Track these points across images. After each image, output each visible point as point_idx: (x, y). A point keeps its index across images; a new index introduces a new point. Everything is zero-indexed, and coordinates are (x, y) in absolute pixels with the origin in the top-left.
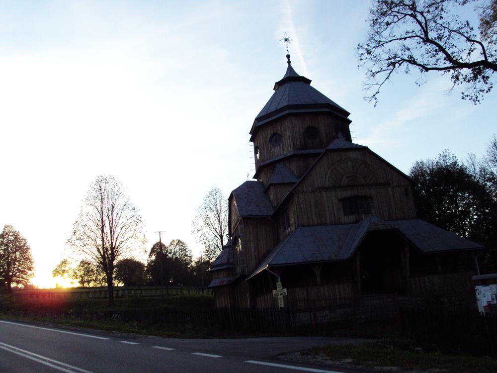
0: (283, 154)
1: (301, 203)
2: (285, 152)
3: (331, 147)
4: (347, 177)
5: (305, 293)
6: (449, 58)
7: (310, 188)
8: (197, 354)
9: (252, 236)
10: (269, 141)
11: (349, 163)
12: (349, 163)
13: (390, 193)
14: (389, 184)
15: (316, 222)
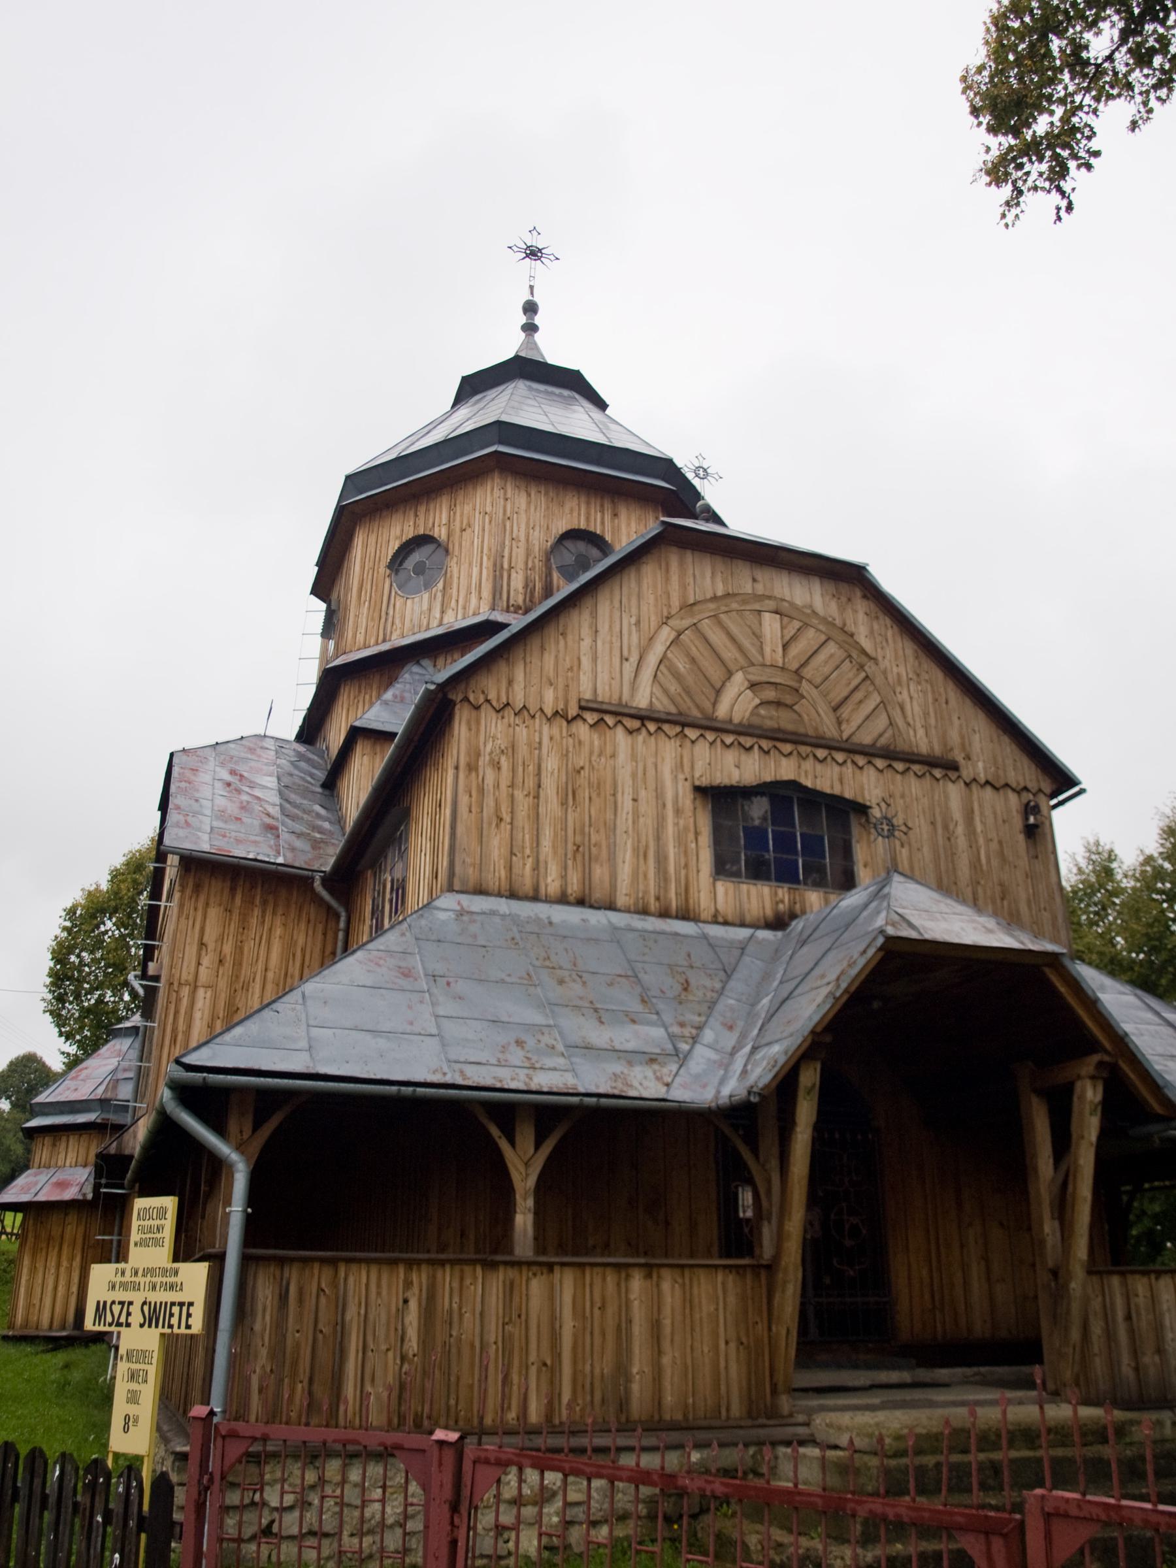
0: (440, 624)
1: (484, 760)
5: (413, 1305)
6: (716, 953)
7: (549, 696)
10: (390, 566)
11: (767, 616)
13: (957, 813)
14: (951, 766)
15: (552, 883)
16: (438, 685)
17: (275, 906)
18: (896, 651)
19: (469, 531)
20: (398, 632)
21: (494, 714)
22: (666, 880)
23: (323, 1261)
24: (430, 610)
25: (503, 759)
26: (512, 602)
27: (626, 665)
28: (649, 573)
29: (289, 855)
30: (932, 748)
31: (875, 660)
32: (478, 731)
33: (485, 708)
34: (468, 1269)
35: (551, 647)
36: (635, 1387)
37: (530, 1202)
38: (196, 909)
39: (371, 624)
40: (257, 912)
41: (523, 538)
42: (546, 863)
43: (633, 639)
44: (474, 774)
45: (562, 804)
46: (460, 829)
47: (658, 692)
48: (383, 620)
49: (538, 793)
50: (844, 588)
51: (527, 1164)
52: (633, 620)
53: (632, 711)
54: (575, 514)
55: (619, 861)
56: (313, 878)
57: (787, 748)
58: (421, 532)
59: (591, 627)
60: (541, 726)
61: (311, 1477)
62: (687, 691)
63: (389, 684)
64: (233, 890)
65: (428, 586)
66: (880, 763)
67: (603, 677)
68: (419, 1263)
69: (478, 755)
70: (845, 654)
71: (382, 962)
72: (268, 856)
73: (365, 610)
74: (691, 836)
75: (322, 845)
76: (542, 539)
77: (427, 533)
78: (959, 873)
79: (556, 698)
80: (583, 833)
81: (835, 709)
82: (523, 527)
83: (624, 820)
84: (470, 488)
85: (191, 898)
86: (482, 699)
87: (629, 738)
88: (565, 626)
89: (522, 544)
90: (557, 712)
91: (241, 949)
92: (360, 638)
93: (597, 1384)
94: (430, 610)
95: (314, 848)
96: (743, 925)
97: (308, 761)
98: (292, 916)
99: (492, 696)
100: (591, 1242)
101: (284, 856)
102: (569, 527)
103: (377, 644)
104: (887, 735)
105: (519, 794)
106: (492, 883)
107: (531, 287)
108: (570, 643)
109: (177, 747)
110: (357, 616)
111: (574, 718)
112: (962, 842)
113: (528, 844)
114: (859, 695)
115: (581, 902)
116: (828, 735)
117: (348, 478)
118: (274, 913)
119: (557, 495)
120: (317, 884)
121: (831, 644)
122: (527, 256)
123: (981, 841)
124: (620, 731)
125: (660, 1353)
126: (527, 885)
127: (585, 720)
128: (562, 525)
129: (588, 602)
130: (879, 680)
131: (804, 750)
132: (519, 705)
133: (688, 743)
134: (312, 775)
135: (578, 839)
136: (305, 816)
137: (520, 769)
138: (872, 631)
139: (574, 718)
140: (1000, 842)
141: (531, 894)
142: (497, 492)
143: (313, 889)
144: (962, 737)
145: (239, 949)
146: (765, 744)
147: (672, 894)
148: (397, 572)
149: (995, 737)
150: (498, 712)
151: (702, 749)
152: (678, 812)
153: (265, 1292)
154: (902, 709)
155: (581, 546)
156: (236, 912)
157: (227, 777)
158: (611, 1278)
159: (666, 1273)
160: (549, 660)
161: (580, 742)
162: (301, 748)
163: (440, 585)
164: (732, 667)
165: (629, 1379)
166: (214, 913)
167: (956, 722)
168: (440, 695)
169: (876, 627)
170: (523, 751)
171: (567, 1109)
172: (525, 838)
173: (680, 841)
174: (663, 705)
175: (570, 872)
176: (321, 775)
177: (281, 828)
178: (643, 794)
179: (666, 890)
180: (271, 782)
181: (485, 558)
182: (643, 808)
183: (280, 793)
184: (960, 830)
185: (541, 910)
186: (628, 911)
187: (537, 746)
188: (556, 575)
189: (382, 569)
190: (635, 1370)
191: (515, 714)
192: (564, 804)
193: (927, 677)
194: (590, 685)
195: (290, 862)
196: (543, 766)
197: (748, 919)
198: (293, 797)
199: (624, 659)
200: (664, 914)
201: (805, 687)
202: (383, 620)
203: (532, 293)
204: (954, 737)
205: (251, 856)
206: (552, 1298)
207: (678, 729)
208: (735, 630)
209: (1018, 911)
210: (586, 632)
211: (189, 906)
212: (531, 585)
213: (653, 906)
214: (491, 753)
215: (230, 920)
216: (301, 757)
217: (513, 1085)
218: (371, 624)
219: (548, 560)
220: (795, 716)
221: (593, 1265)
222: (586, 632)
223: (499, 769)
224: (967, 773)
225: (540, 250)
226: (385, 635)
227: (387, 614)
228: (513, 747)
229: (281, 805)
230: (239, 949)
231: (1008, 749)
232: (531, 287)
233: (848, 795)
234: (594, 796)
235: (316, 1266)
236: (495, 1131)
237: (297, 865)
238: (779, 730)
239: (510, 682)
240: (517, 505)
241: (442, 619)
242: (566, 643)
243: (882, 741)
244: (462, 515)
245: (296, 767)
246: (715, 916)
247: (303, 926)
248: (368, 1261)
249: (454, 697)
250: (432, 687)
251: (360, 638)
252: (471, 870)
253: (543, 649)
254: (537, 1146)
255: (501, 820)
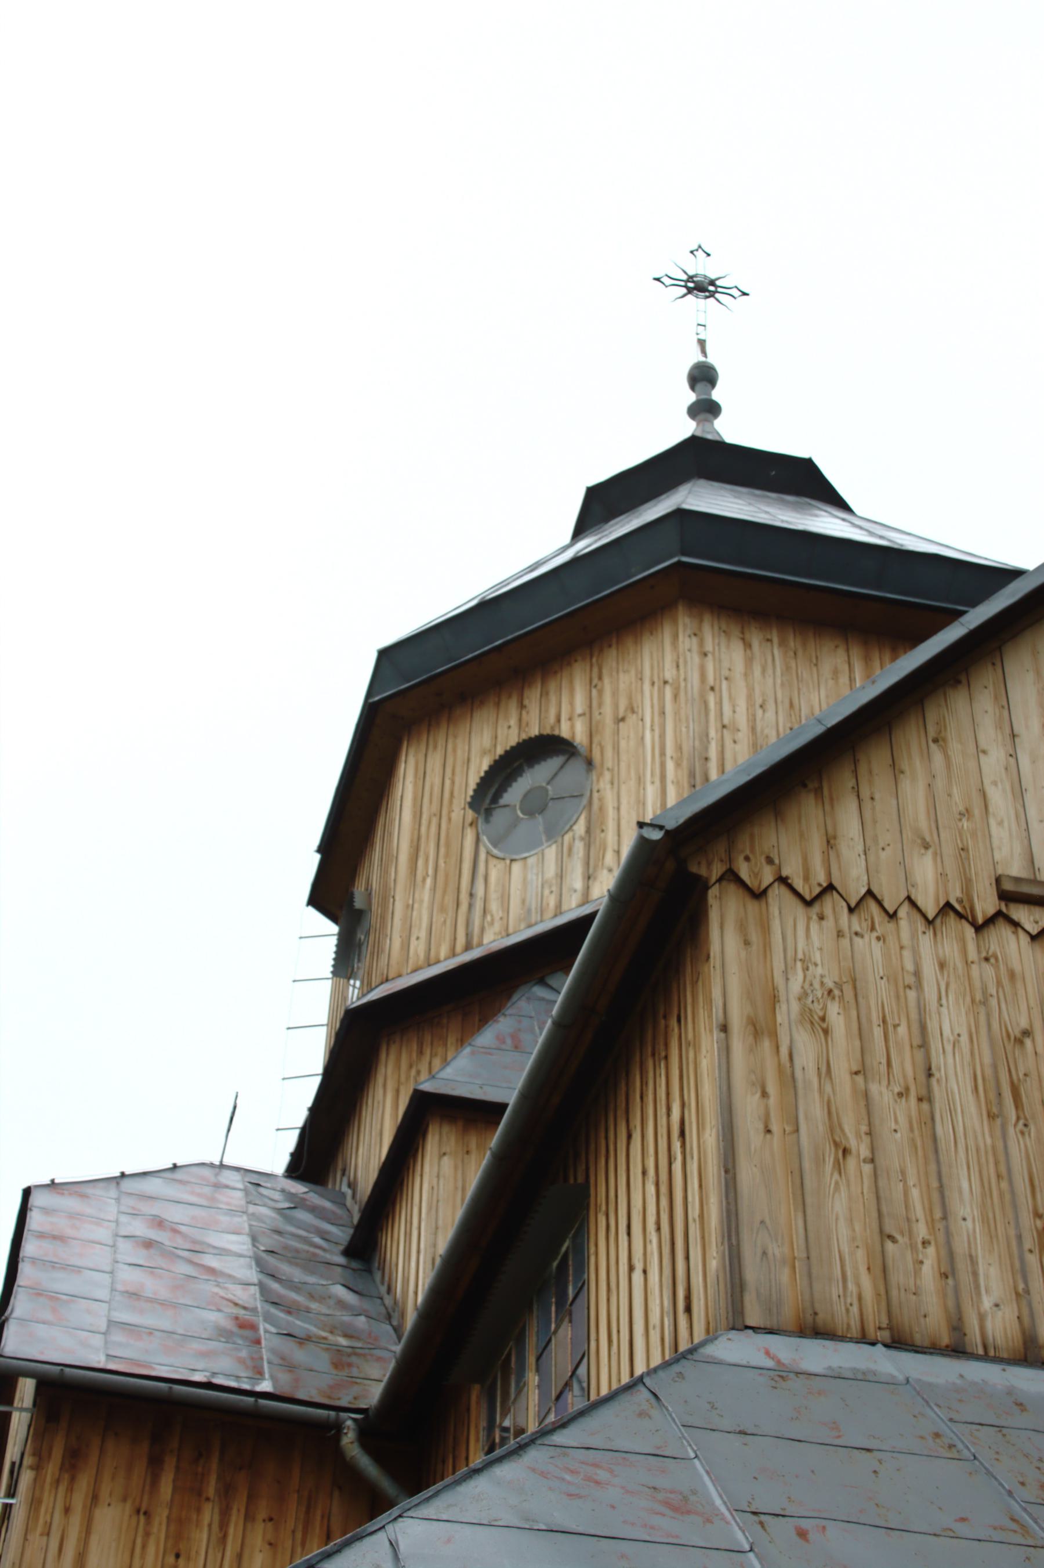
1: (788, 1011)
16: (667, 832)
17: (251, 1498)
19: (632, 719)
20: (497, 926)
21: (800, 909)
24: (561, 876)
25: (833, 1010)
29: (284, 1377)
32: (767, 946)
33: (779, 898)
38: (67, 1510)
39: (438, 919)
40: (209, 1514)
42: (973, 1260)
44: (766, 1044)
45: (991, 1116)
46: (747, 1174)
48: (464, 907)
49: (929, 1087)
54: (844, 679)
56: (338, 1428)
58: (534, 731)
59: (999, 726)
60: (914, 936)
63: (485, 1020)
64: (155, 1463)
65: (553, 833)
69: (774, 1000)
71: (602, 1475)
72: (238, 1378)
73: (425, 894)
75: (354, 1359)
77: (547, 731)
84: (629, 642)
85: (57, 1482)
88: (941, 726)
90: (948, 905)
92: (418, 948)
94: (561, 876)
95: (337, 1365)
97: (313, 1210)
98: (291, 1524)
99: (792, 869)
101: (273, 1378)
103: (454, 954)
105: (882, 1094)
106: (845, 1316)
107: (702, 343)
108: (956, 758)
109: (40, 1177)
110: (409, 907)
111: (990, 921)
113: (919, 1211)
117: (384, 655)
118: (249, 1517)
119: (804, 645)
120: (349, 1439)
122: (690, 291)
127: (1016, 925)
132: (856, 890)
134: (323, 1235)
136: (314, 1306)
137: (878, 1032)
139: (990, 921)
141: (945, 1340)
142: (686, 642)
143: (338, 1452)
148: (488, 813)
150: (808, 903)
156: (161, 1516)
157: (140, 1228)
161: (1012, 975)
162: (298, 1188)
163: (580, 828)
168: (670, 865)
176: (343, 1235)
177: (263, 1326)
180: (240, 1243)
181: (670, 766)
183: (259, 1263)
187: (910, 980)
189: (460, 811)
191: (851, 910)
194: (1018, 849)
195: (286, 1390)
196: (932, 1026)
198: (286, 1269)
202: (464, 907)
203: (704, 352)
205: (198, 1377)
210: (989, 734)
211: (52, 1501)
214: (803, 996)
215: (147, 1534)
216: (298, 1203)
218: (438, 919)
222: (989, 734)
223: (826, 1032)
225: (712, 283)
226: (469, 936)
227: (471, 895)
228: (854, 981)
229: (261, 1285)
232: (702, 343)
237: (301, 1395)
239: (830, 842)
240: (726, 664)
241: (587, 889)
242: (947, 757)
244: (615, 694)
245: (289, 1220)
249: (703, 872)
250: (656, 835)
251: (418, 948)
252: (785, 1276)
255: (846, 1152)
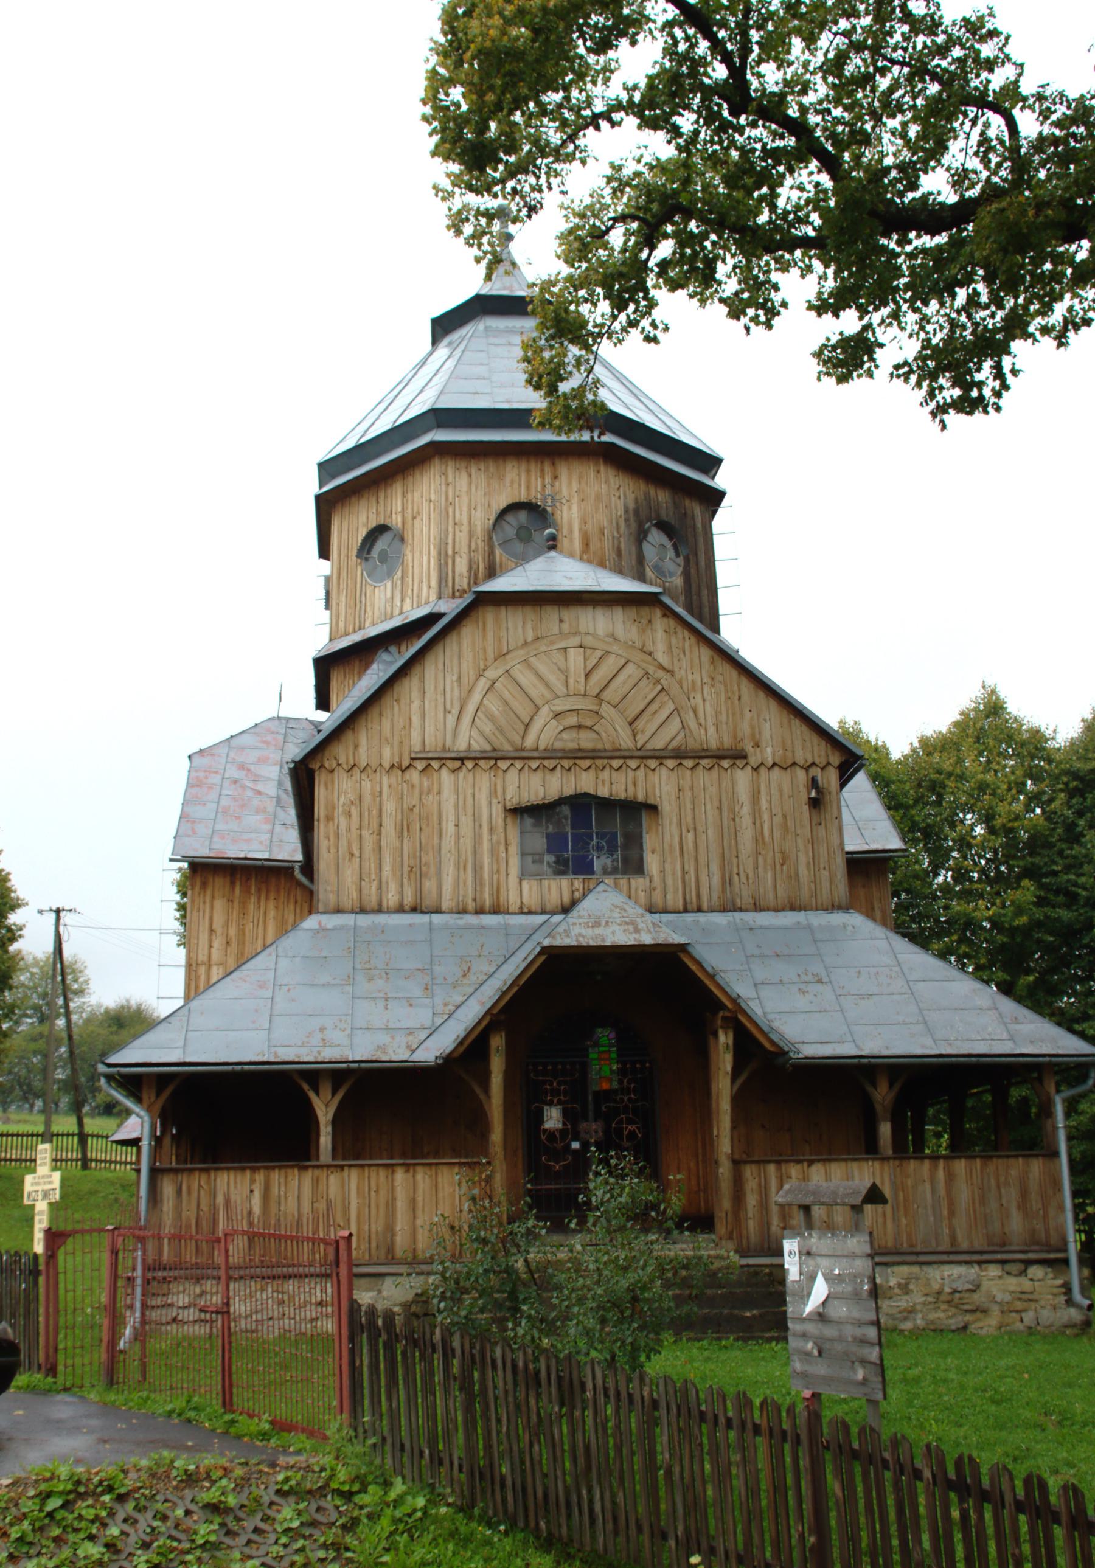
2: (407, 606)
3: (502, 584)
4: (557, 715)
7: (387, 753)
8: (633, 1425)
9: (217, 943)
10: (359, 555)
11: (571, 651)
12: (575, 658)
14: (738, 756)
15: (391, 898)
17: (268, 892)
18: (692, 660)
22: (482, 885)
23: (201, 1170)
26: (457, 587)
27: (449, 716)
28: (468, 633)
30: (722, 743)
31: (671, 673)
34: (290, 1171)
35: (387, 712)
36: (398, 1239)
37: (330, 1129)
40: (253, 899)
41: (465, 521)
43: (454, 694)
47: (475, 733)
50: (645, 611)
51: (327, 1105)
52: (455, 678)
53: (453, 755)
54: (516, 485)
55: (444, 876)
56: (293, 868)
57: (587, 763)
61: (198, 1291)
62: (500, 730)
64: (233, 883)
65: (390, 574)
66: (671, 763)
67: (430, 730)
68: (258, 1168)
69: (334, 808)
70: (641, 673)
73: (343, 599)
74: (502, 848)
76: (483, 519)
78: (741, 847)
79: (393, 754)
80: (415, 857)
81: (631, 724)
82: (465, 509)
83: (448, 842)
86: (334, 764)
87: (452, 776)
89: (465, 528)
91: (243, 931)
93: (373, 1236)
96: (543, 912)
100: (426, 1150)
102: (510, 501)
104: (679, 738)
105: (366, 833)
106: (347, 904)
112: (746, 820)
114: (654, 707)
115: (414, 910)
116: (624, 746)
118: (267, 898)
120: (297, 873)
121: (630, 666)
123: (766, 817)
124: (444, 772)
125: (415, 1218)
126: (372, 901)
128: (502, 501)
129: (416, 671)
130: (675, 690)
131: (599, 762)
133: (500, 773)
135: (412, 863)
138: (670, 647)
140: (785, 816)
144: (752, 727)
145: (241, 932)
146: (566, 763)
147: (487, 896)
149: (785, 721)
151: (512, 776)
152: (491, 830)
153: (168, 1188)
154: (695, 711)
155: (523, 516)
158: (382, 1173)
159: (420, 1169)
160: (386, 724)
163: (399, 574)
164: (539, 702)
165: (393, 1234)
166: (220, 904)
167: (748, 715)
169: (674, 641)
170: (367, 799)
171: (348, 1072)
172: (371, 865)
173: (493, 852)
174: (479, 744)
175: (405, 888)
178: (463, 819)
179: (482, 892)
182: (463, 830)
184: (746, 810)
185: (381, 919)
186: (451, 912)
188: (498, 552)
190: (398, 1228)
192: (401, 836)
193: (721, 678)
194: (420, 739)
197: (548, 908)
199: (446, 712)
200: (480, 911)
201: (606, 709)
204: (745, 729)
205: (242, 855)
206: (343, 1186)
207: (492, 762)
208: (542, 669)
209: (797, 874)
210: (415, 694)
212: (474, 567)
213: (471, 906)
217: (306, 1059)
219: (490, 538)
220: (594, 735)
221: (370, 1165)
222: (415, 694)
224: (753, 761)
230: (241, 932)
231: (799, 728)
233: (641, 798)
234: (424, 826)
235: (197, 1174)
236: (305, 1087)
238: (580, 750)
239: (356, 747)
243: (674, 744)
246: (521, 908)
247: (292, 907)
248: (228, 1169)
253: (381, 715)
254: (333, 1095)
